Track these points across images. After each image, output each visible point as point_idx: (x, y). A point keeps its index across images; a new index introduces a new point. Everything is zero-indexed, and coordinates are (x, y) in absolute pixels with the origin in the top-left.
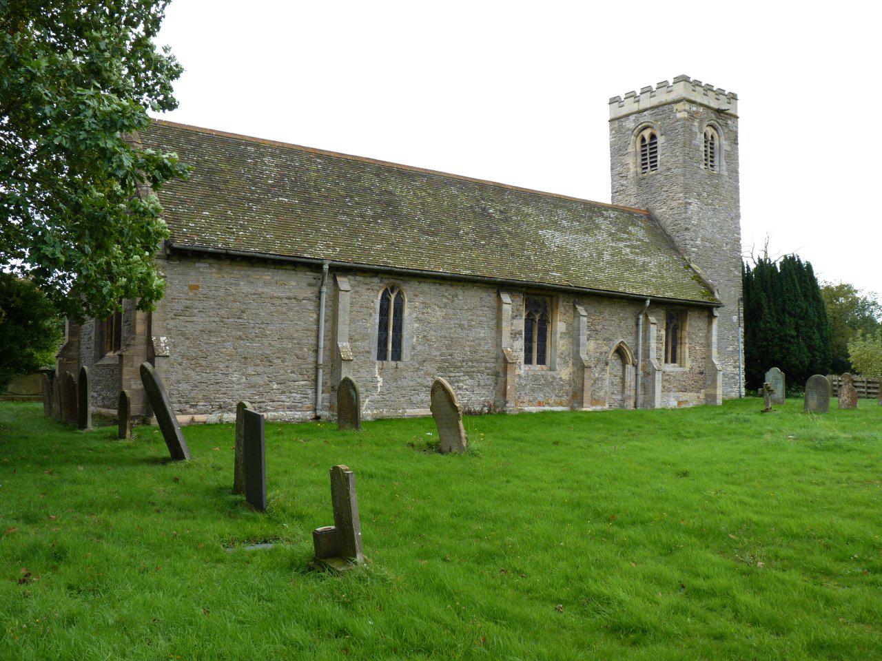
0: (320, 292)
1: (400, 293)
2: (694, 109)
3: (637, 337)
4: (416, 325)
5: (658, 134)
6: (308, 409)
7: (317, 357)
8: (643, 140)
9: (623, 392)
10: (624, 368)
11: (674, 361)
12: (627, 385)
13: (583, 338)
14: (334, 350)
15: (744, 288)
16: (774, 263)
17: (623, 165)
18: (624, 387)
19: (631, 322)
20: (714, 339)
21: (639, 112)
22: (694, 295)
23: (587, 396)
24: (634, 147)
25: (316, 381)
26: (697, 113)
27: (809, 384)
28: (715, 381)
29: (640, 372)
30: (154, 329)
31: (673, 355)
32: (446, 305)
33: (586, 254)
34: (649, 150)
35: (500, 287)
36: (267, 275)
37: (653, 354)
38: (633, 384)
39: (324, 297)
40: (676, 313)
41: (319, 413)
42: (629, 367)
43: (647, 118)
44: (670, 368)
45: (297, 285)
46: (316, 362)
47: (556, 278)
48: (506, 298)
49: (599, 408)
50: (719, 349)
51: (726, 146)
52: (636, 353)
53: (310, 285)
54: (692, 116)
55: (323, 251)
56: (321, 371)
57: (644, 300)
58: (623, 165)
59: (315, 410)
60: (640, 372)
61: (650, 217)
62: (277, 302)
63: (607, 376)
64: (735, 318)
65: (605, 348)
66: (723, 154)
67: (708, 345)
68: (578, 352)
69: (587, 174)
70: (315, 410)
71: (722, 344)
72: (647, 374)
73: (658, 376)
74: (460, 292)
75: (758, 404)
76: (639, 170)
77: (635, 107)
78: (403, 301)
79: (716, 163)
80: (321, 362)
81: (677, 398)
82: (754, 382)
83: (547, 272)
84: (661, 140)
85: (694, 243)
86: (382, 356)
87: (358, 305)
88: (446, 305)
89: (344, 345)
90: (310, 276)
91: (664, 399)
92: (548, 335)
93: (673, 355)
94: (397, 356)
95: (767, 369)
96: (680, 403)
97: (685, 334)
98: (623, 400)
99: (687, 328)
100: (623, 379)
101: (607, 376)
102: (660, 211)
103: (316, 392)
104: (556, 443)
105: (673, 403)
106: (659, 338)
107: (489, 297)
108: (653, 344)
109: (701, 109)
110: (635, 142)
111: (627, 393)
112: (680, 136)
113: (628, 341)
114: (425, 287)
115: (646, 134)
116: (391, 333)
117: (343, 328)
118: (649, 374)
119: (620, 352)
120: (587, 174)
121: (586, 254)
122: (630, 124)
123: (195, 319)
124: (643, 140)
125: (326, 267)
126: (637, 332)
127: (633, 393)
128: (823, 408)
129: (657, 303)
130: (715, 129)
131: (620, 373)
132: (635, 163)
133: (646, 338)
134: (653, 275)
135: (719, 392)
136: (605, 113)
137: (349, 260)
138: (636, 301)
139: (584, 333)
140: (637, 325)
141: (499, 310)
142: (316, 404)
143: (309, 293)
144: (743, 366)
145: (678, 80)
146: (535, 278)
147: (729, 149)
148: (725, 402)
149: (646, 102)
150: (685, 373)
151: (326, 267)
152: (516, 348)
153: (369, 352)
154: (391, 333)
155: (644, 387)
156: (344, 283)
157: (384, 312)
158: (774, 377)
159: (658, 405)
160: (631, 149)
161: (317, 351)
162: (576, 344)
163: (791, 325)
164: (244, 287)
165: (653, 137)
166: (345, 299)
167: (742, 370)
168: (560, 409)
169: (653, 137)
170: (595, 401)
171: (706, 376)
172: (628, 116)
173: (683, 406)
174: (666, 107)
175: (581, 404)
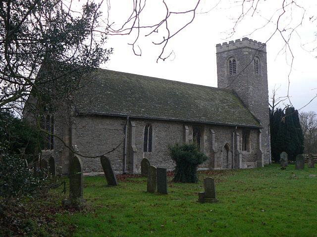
0: (125, 127)
1: (151, 127)
2: (250, 50)
3: (232, 141)
4: (156, 138)
5: (236, 60)
6: (121, 170)
7: (124, 151)
8: (230, 62)
9: (227, 162)
10: (228, 153)
11: (245, 150)
12: (229, 159)
13: (213, 142)
14: (130, 148)
15: (270, 120)
16: (283, 111)
17: (222, 71)
18: (228, 160)
19: (230, 135)
20: (260, 141)
21: (229, 51)
22: (253, 124)
23: (216, 163)
24: (226, 65)
25: (124, 160)
26: (251, 52)
27: (297, 158)
28: (261, 157)
29: (234, 154)
30: (73, 142)
31: (245, 148)
32: (166, 130)
33: (213, 109)
34: (232, 65)
35: (184, 123)
36: (108, 121)
37: (238, 147)
38: (231, 159)
39: (127, 129)
40: (246, 131)
41: (126, 171)
42: (230, 152)
43: (232, 53)
44: (244, 152)
45: (117, 125)
46: (124, 153)
47: (203, 119)
48: (187, 127)
49: (219, 168)
50: (262, 144)
51: (262, 64)
52: (232, 147)
53: (122, 125)
54: (250, 53)
55: (124, 113)
56: (126, 156)
57: (235, 127)
58: (222, 71)
59: (124, 170)
60: (234, 154)
61: (234, 93)
62: (111, 131)
63: (222, 156)
64: (267, 132)
65: (221, 146)
66: (261, 67)
67: (258, 143)
68: (212, 147)
69: (205, 74)
70: (124, 170)
71: (264, 143)
72: (236, 155)
73: (241, 156)
74: (171, 126)
75: (278, 168)
76: (229, 74)
77: (227, 49)
78: (152, 129)
79: (259, 71)
80: (125, 153)
81: (247, 164)
82: (276, 157)
83: (200, 117)
84: (237, 62)
85: (251, 103)
86: (145, 150)
87: (138, 130)
88: (166, 130)
89: (134, 146)
90: (121, 122)
91: (243, 165)
92: (201, 141)
93: (245, 148)
94: (150, 150)
95: (281, 152)
96: (248, 166)
97: (250, 139)
98: (227, 165)
99: (250, 137)
100: (227, 157)
101: (222, 156)
102: (238, 90)
103: (124, 164)
104: (172, 192)
105: (246, 167)
106: (240, 141)
107: (180, 127)
108: (238, 144)
109: (253, 51)
110: (227, 63)
111: (229, 162)
112: (243, 61)
113: (229, 142)
114: (159, 124)
115: (232, 59)
116: (148, 141)
117: (133, 140)
118: (237, 155)
119: (226, 147)
120: (205, 74)
121: (213, 109)
122: (225, 55)
123: (85, 138)
124: (230, 62)
125: (128, 118)
126: (232, 139)
127: (231, 162)
128: (302, 168)
129: (240, 128)
130: (258, 58)
131: (226, 155)
132: (227, 71)
133: (236, 141)
134: (236, 117)
135: (263, 162)
136: (214, 51)
137: (134, 115)
138: (231, 128)
139: (214, 139)
140: (232, 136)
141: (184, 132)
142: (124, 168)
143: (121, 128)
144: (270, 151)
145: (244, 39)
146: (197, 120)
147: (263, 65)
148: (265, 166)
149: (231, 47)
150: (249, 154)
151: (128, 118)
152: (239, 145)
153: (141, 149)
154: (148, 141)
155: (235, 161)
156: (133, 124)
157: (146, 134)
158: (284, 155)
159: (241, 167)
160: (225, 65)
161: (124, 149)
162: (211, 144)
163: (286, 127)
164: (101, 126)
165: (234, 61)
166: (134, 129)
167: (270, 153)
168: (206, 169)
169: (234, 61)
170: (218, 166)
171: (257, 156)
172: (224, 52)
173: (249, 168)
174: (240, 50)
175: (214, 167)
